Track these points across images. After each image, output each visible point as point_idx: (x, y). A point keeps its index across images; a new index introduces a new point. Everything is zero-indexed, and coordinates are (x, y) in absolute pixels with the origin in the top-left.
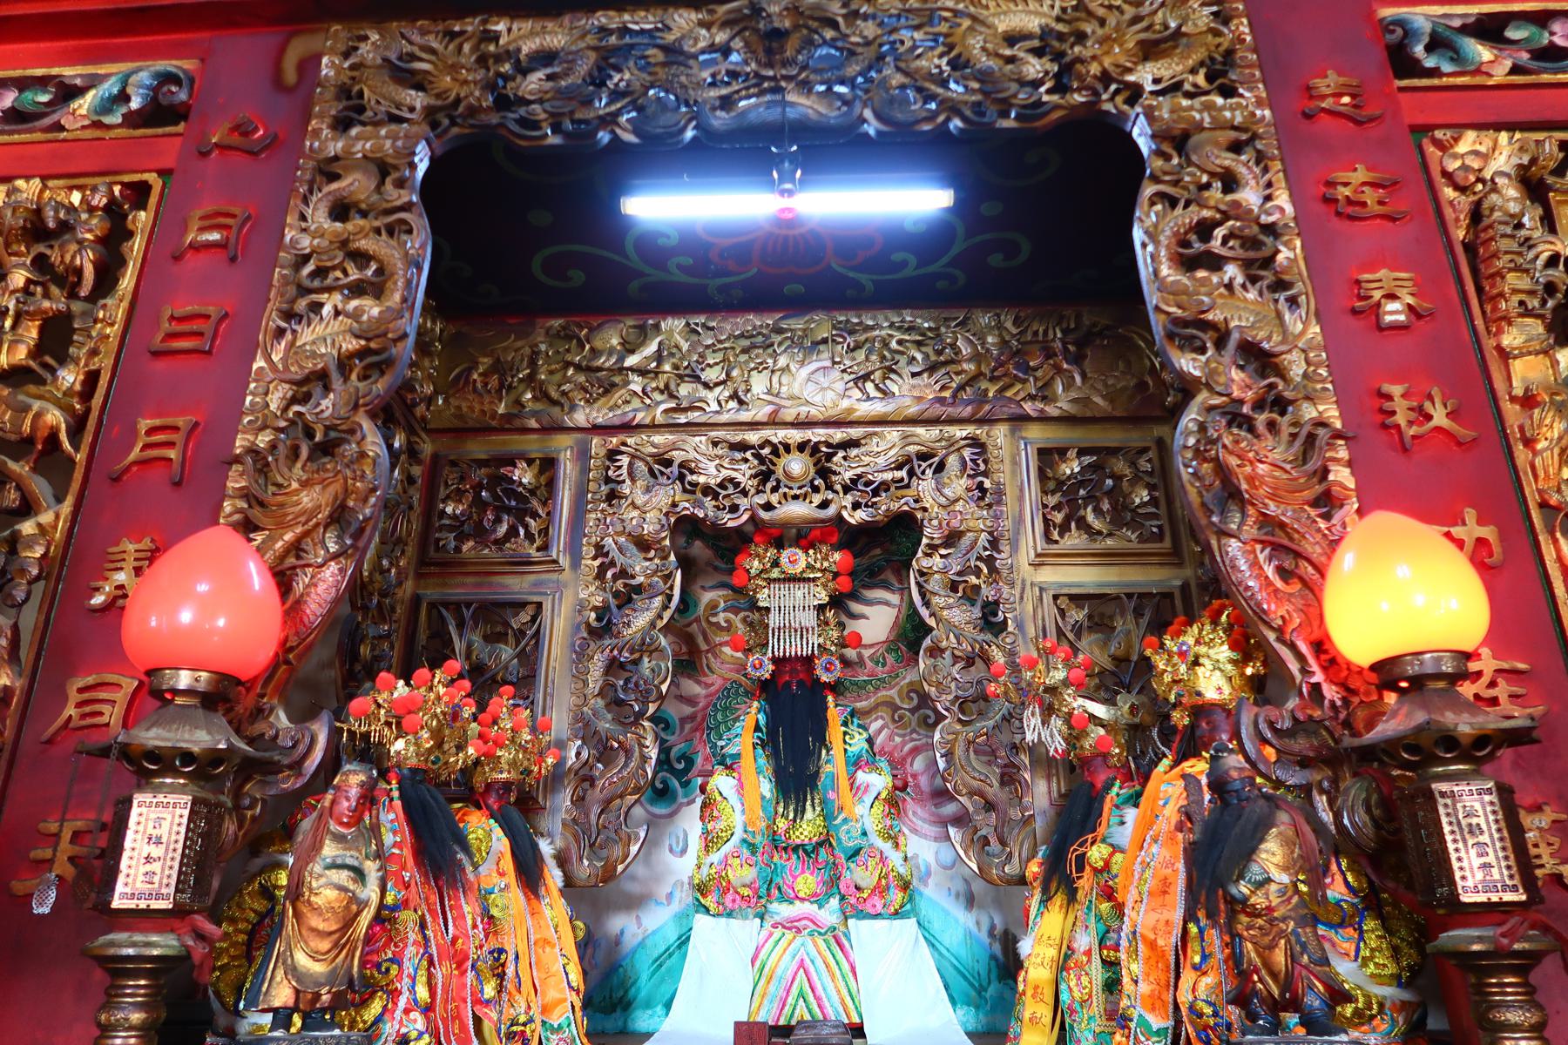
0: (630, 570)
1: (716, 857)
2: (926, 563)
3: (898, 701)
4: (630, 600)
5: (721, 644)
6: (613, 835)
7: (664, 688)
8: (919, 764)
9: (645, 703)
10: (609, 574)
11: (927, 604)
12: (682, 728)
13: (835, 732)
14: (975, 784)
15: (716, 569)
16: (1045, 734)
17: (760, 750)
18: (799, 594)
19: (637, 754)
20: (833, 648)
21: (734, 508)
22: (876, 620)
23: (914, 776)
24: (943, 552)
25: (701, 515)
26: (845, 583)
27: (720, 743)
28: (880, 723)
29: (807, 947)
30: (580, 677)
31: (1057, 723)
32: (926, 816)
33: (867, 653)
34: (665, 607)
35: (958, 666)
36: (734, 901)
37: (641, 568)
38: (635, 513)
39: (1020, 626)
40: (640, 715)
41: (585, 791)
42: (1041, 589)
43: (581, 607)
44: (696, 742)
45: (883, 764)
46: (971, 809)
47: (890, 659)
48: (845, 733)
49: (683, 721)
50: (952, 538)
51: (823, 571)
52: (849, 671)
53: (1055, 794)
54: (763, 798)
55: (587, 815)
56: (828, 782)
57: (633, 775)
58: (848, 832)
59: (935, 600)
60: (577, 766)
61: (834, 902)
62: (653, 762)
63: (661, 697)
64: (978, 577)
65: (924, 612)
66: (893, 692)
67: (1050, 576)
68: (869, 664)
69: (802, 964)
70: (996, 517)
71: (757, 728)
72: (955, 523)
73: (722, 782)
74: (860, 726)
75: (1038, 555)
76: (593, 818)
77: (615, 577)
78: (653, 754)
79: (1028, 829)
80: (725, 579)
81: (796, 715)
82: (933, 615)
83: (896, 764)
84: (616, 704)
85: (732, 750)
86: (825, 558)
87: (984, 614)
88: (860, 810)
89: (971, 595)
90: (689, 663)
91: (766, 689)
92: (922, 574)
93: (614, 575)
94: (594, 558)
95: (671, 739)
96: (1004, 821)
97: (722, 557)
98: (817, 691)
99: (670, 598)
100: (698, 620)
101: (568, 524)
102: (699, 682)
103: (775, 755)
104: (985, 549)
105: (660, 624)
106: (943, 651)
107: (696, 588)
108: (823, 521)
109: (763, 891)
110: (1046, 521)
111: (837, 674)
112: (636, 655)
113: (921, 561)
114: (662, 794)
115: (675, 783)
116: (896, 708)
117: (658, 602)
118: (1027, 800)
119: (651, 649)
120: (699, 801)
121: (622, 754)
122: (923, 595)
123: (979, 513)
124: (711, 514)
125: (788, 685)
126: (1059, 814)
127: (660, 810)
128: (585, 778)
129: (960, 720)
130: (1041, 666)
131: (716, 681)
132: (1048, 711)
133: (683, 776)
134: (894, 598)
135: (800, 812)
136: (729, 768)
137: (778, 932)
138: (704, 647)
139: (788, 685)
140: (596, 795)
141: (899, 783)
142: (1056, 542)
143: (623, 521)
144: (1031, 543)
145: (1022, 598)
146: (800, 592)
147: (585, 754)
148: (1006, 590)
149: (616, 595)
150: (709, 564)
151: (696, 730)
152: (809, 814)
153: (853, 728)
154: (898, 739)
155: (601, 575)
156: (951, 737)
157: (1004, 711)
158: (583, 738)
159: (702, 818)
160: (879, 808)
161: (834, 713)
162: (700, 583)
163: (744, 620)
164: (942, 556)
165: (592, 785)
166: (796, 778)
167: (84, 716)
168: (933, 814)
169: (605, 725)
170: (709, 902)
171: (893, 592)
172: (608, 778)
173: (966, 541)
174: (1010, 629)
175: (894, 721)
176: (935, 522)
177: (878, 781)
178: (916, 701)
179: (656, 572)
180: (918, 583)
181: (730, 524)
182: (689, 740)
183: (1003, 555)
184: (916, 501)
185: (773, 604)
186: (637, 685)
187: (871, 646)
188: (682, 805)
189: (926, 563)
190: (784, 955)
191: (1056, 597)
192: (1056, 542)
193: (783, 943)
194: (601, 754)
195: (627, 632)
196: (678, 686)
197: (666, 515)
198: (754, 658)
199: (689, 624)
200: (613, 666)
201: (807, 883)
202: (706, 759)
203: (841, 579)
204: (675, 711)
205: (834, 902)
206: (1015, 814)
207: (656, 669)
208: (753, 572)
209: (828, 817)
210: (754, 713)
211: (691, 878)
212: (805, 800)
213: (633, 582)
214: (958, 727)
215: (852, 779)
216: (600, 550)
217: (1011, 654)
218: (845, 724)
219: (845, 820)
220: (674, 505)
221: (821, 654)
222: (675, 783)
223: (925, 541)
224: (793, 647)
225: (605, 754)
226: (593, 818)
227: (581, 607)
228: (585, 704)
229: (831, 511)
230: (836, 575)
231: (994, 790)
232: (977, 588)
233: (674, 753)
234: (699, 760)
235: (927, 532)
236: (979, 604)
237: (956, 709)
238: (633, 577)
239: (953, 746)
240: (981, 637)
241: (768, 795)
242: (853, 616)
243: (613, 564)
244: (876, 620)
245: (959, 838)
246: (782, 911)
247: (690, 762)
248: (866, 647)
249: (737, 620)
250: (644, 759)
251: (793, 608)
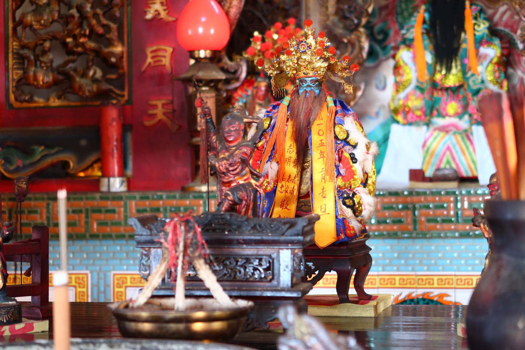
1: (402, 95)
9: (359, 19)
13: (469, 23)
29: (450, 139)
36: (412, 118)
40: (358, 25)
54: (427, 63)
57: (357, 57)
61: (466, 117)
69: (448, 148)
71: (424, 22)
84: (344, 18)
88: (480, 69)
109: (428, 112)
135: (449, 69)
137: (436, 133)
152: (454, 71)
167: (155, 62)
170: (400, 118)
182: (385, 21)
190: (439, 142)
193: (439, 138)
201: (452, 107)
205: (466, 117)
209: (464, 72)
211: (389, 106)
218: (476, 18)
219: (473, 75)
246: (439, 121)
250: (361, 48)
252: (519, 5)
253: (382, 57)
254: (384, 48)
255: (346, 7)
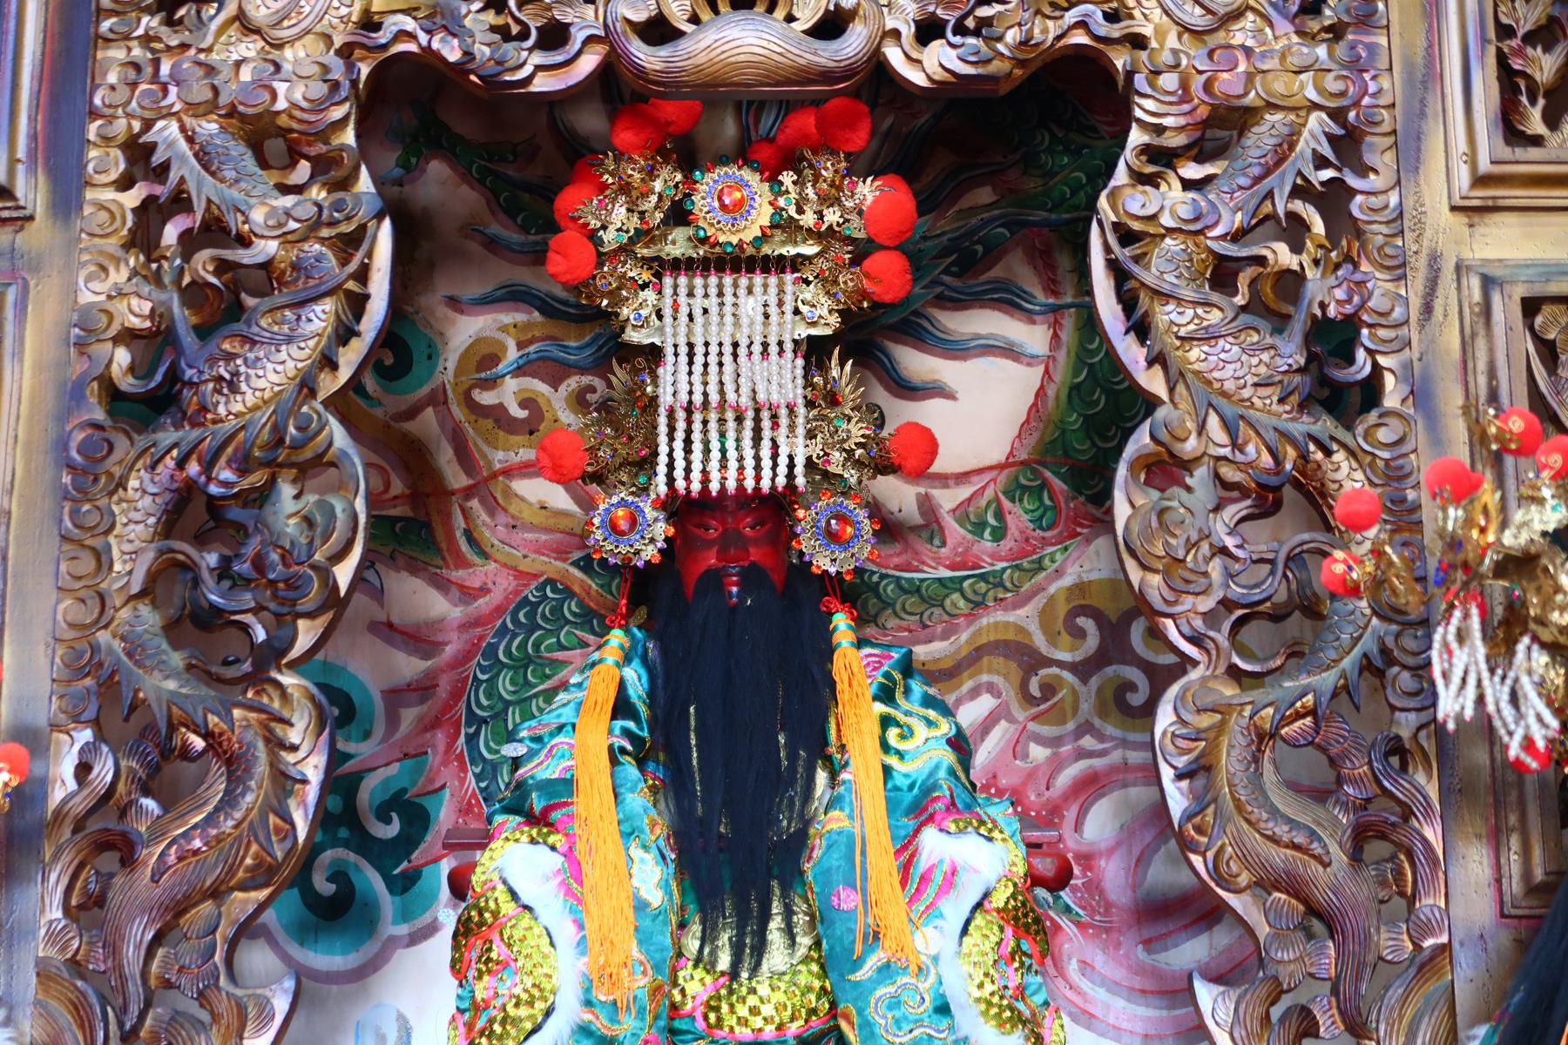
0: (234, 222)
2: (1139, 202)
3: (1040, 641)
4: (236, 311)
5: (508, 472)
6: (194, 1009)
7: (343, 574)
8: (1100, 824)
9: (284, 621)
10: (171, 233)
11: (1141, 329)
12: (393, 720)
13: (856, 717)
14: (1278, 857)
15: (493, 245)
16: (1498, 695)
17: (630, 770)
18: (750, 307)
19: (262, 768)
20: (851, 476)
21: (554, 36)
22: (981, 398)
23: (1087, 859)
24: (1192, 171)
25: (453, 54)
26: (888, 274)
27: (510, 750)
28: (986, 703)
30: (87, 541)
31: (1532, 661)
32: (1119, 974)
33: (947, 499)
34: (344, 334)
35: (1232, 512)
37: (268, 213)
38: (249, 48)
39: (1420, 394)
40: (274, 653)
41: (106, 879)
42: (1488, 282)
43: (86, 331)
44: (434, 759)
45: (1000, 811)
46: (1263, 930)
47: (1019, 517)
48: (886, 722)
49: (396, 697)
50: (1221, 128)
51: (826, 236)
52: (893, 553)
53: (1514, 885)
54: (641, 906)
55: (113, 949)
56: (835, 859)
57: (253, 830)
58: (895, 1002)
59: (1165, 315)
60: (80, 805)
62: (312, 793)
63: (333, 602)
64: (1297, 249)
65: (1131, 353)
66: (1025, 616)
67: (1518, 244)
68: (955, 531)
70: (1356, 66)
71: (622, 707)
72: (1229, 83)
73: (517, 863)
74: (928, 701)
75: (1480, 181)
76: (132, 956)
77: (190, 244)
78: (313, 769)
79: (1433, 986)
80: (524, 276)
81: (739, 668)
82: (1157, 359)
83: (1040, 823)
84: (197, 624)
85: (546, 769)
86: (827, 200)
87: (1311, 358)
88: (934, 939)
89: (1275, 300)
90: (414, 527)
91: (646, 594)
92: (1127, 236)
93: (185, 237)
94: (125, 183)
95: (361, 750)
96: (1360, 963)
97: (511, 211)
98: (806, 596)
99: (358, 303)
100: (437, 399)
101: (36, 96)
102: (442, 585)
103: (674, 786)
104: (1321, 162)
105: (330, 384)
106: (1188, 465)
107: (432, 301)
108: (826, 76)
110: (1508, 78)
111: (864, 550)
112: (257, 478)
113: (1125, 198)
114: (336, 912)
115: (372, 880)
116: (1031, 661)
117: (321, 317)
118: (1430, 902)
119: (313, 466)
120: (448, 917)
121: (217, 770)
122: (1128, 302)
123: (1303, 52)
124: (482, 51)
125: (714, 580)
126: (1522, 945)
127: (326, 958)
128: (107, 839)
129: (1234, 673)
130: (1488, 495)
131: (493, 580)
132: (1507, 629)
133: (398, 862)
134: (1033, 337)
135: (750, 949)
136: (539, 821)
138: (457, 479)
139: (714, 580)
140: (138, 892)
141: (1045, 866)
142: (1537, 141)
143: (210, 70)
144: (1460, 143)
145: (1428, 309)
146: (751, 305)
147: (104, 771)
148: (1380, 288)
149: (194, 293)
150: (471, 229)
151: (433, 724)
152: (777, 956)
153: (909, 707)
154: (1038, 753)
155: (143, 237)
156: (1205, 721)
157: (1368, 644)
158: (96, 724)
159: (458, 968)
160: (987, 936)
161: (853, 663)
162: (444, 286)
163: (580, 401)
164: (1187, 185)
165: (129, 860)
166: (739, 849)
168: (1141, 970)
169: (164, 682)
171: (1030, 317)
172: (173, 840)
173: (1262, 138)
174: (1391, 400)
175: (1027, 699)
176: (1169, 81)
177: (985, 859)
178: (1092, 641)
179: (313, 227)
180: (1113, 266)
181: (542, 84)
183: (1373, 181)
184: (1112, 17)
185: (669, 336)
186: (259, 564)
187: (963, 477)
188: (392, 943)
189: (1139, 202)
191: (1531, 307)
192: (1537, 141)
194: (154, 770)
195: (229, 408)
196: (378, 594)
197: (346, 52)
198: (611, 502)
199: (413, 412)
200: (190, 513)
202: (466, 810)
203: (880, 262)
204: (373, 668)
206: (1393, 943)
207: (323, 518)
208: (610, 237)
209: (830, 961)
210: (614, 665)
212: (765, 917)
213: (244, 256)
214: (1229, 691)
215: (906, 850)
216: (141, 158)
217: (1395, 475)
218: (886, 694)
219: (886, 970)
220: (369, 23)
221: (816, 490)
222: (372, 880)
223: (1136, 137)
224: (725, 465)
225: (161, 758)
226: (132, 956)
227: (86, 331)
228: (103, 622)
229: (853, 44)
230: (861, 252)
231: (1333, 874)
232: (1291, 282)
233: (370, 791)
234: (444, 814)
235: (1145, 107)
236: (1298, 326)
237: (1222, 638)
238: (244, 241)
239: (1213, 746)
240: (1301, 426)
241: (655, 898)
242: (908, 390)
243: (180, 201)
244: (981, 398)
245: (1225, 1012)
247: (416, 818)
248: (944, 480)
249: (557, 401)
250: (285, 782)
251: (733, 362)
252: (1166, 574)
253: (393, 928)
254: (404, 884)
255: (212, 559)
